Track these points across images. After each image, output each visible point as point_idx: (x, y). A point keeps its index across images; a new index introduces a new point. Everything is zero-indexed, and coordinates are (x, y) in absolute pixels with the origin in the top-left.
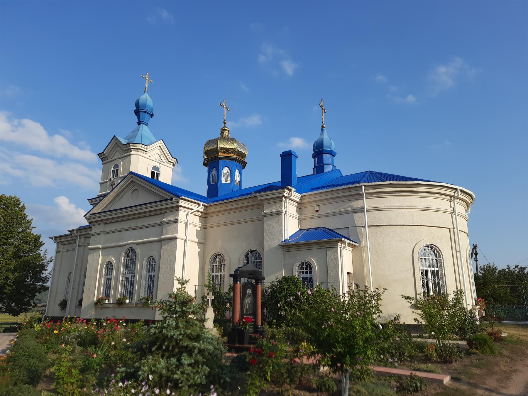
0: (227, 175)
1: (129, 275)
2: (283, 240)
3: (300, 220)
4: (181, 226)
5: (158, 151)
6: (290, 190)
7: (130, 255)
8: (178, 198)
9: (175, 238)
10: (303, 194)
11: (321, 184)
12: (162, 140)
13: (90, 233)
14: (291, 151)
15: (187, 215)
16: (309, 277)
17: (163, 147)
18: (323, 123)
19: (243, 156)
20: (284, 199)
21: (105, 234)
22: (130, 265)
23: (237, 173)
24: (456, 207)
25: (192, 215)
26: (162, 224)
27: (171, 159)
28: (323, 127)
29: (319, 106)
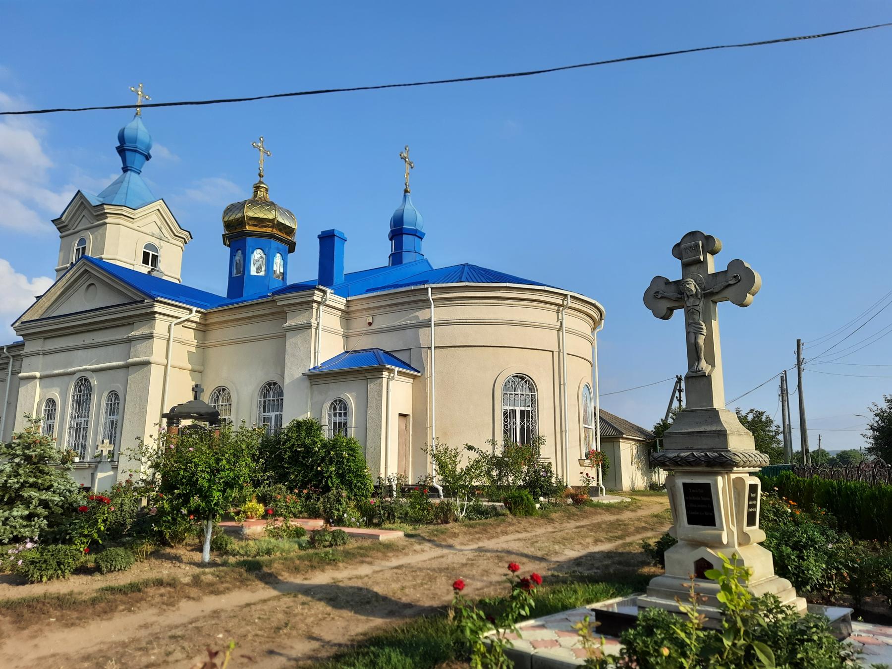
0: (260, 262)
1: (80, 419)
2: (312, 367)
3: (346, 337)
4: (158, 345)
5: (155, 217)
6: (324, 292)
7: (83, 388)
8: (152, 300)
9: (148, 363)
10: (350, 298)
11: (391, 283)
12: (162, 199)
13: (21, 352)
14: (333, 230)
15: (170, 326)
16: (343, 421)
17: (164, 210)
18: (406, 184)
19: (290, 231)
20: (315, 305)
21: (44, 354)
22: (82, 402)
23: (278, 260)
24: (564, 321)
25: (180, 326)
26: (129, 341)
27: (178, 232)
28: (406, 191)
29: (400, 157)
